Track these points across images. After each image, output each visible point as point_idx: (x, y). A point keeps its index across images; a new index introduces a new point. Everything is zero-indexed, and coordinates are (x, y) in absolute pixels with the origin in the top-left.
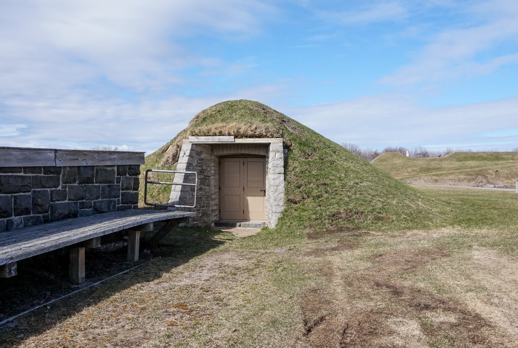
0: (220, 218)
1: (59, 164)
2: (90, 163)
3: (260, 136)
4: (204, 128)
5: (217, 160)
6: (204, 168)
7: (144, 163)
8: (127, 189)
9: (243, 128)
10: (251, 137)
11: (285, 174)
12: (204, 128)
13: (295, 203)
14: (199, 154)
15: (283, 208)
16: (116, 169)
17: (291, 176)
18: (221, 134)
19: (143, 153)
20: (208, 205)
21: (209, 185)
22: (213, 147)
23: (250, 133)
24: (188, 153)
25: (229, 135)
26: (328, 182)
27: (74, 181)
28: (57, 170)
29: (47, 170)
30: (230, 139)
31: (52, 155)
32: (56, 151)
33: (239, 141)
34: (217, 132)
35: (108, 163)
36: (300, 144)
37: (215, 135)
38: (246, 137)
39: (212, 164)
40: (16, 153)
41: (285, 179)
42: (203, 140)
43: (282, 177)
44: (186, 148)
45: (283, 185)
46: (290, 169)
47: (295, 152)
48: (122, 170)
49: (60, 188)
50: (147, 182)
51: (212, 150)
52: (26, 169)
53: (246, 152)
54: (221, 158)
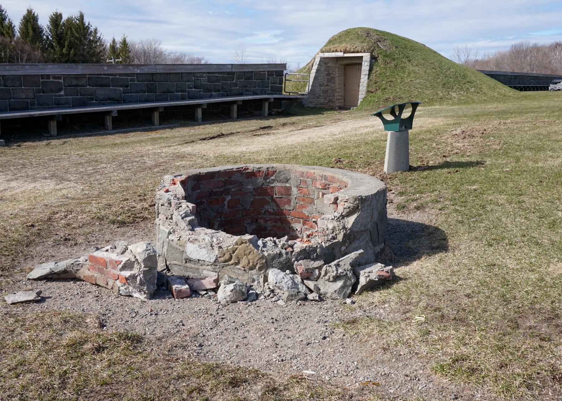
0: (344, 105)
1: (233, 71)
2: (250, 70)
3: (358, 52)
4: (332, 47)
5: (343, 67)
6: (330, 72)
7: (286, 69)
8: (274, 83)
9: (349, 47)
10: (353, 52)
11: (369, 75)
12: (332, 47)
13: (372, 93)
14: (325, 64)
15: (364, 96)
16: (266, 73)
17: (373, 76)
18: (336, 51)
19: (284, 66)
20: (333, 95)
21: (334, 83)
22: (338, 59)
23: (352, 50)
24: (318, 63)
25: (341, 51)
26: (394, 79)
27: (242, 78)
28: (233, 73)
29: (228, 73)
30: (340, 54)
31: (231, 66)
32: (232, 65)
33: (346, 55)
34: (335, 50)
35: (261, 70)
36: (384, 56)
37: (333, 51)
38: (350, 53)
39: (337, 70)
40: (215, 66)
41: (368, 79)
42: (327, 55)
43: (367, 77)
44: (318, 60)
45: (366, 82)
46: (373, 72)
47: (380, 61)
48: (270, 74)
49: (234, 81)
50: (285, 80)
51: (337, 61)
52: (219, 73)
53: (355, 62)
54: (346, 65)
